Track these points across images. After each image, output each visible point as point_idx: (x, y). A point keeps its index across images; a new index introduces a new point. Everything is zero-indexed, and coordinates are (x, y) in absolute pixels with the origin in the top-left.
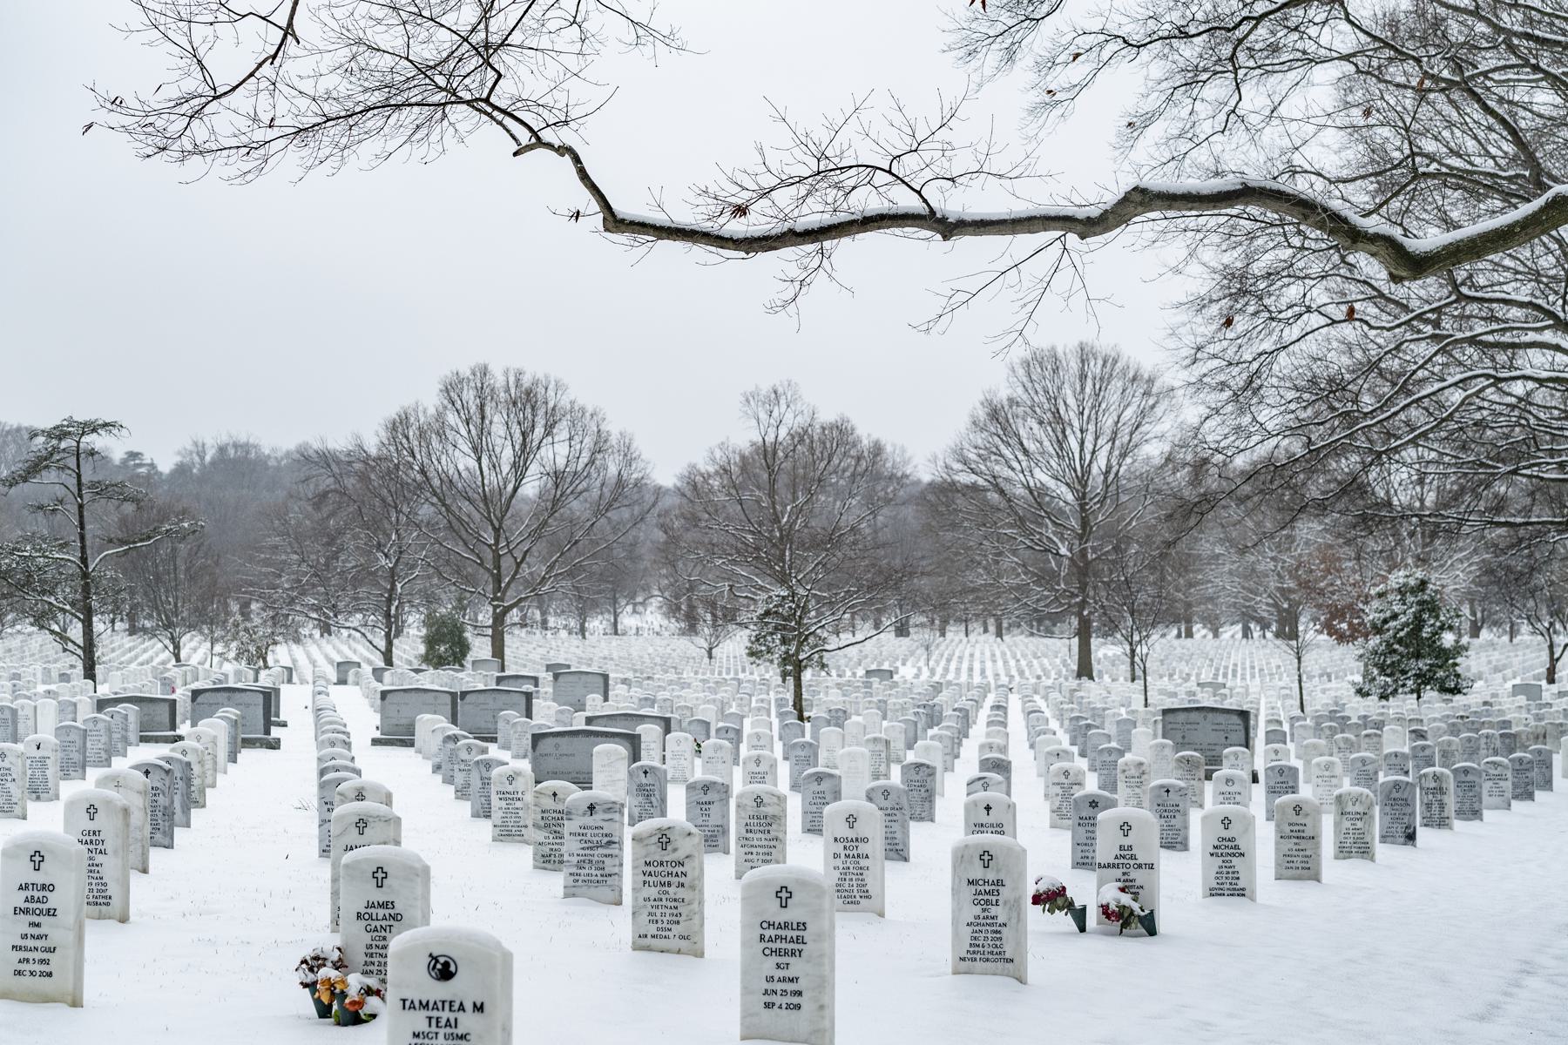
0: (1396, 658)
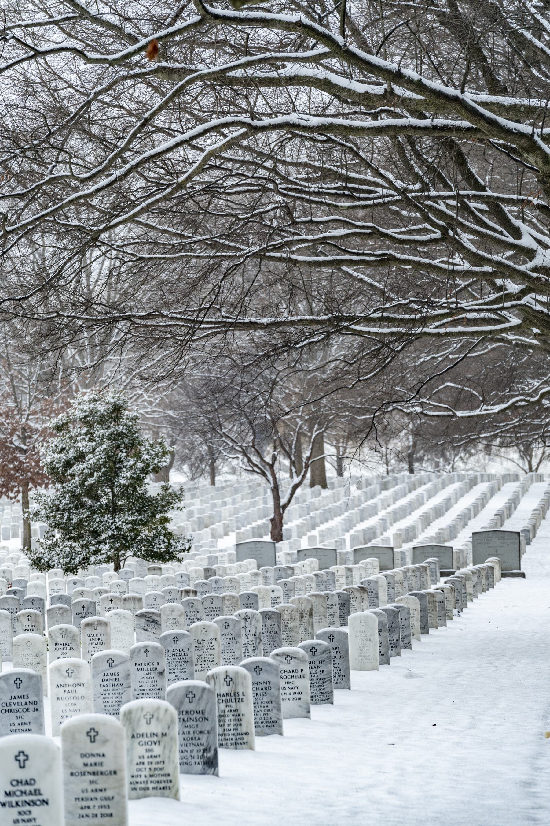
0: (84, 514)
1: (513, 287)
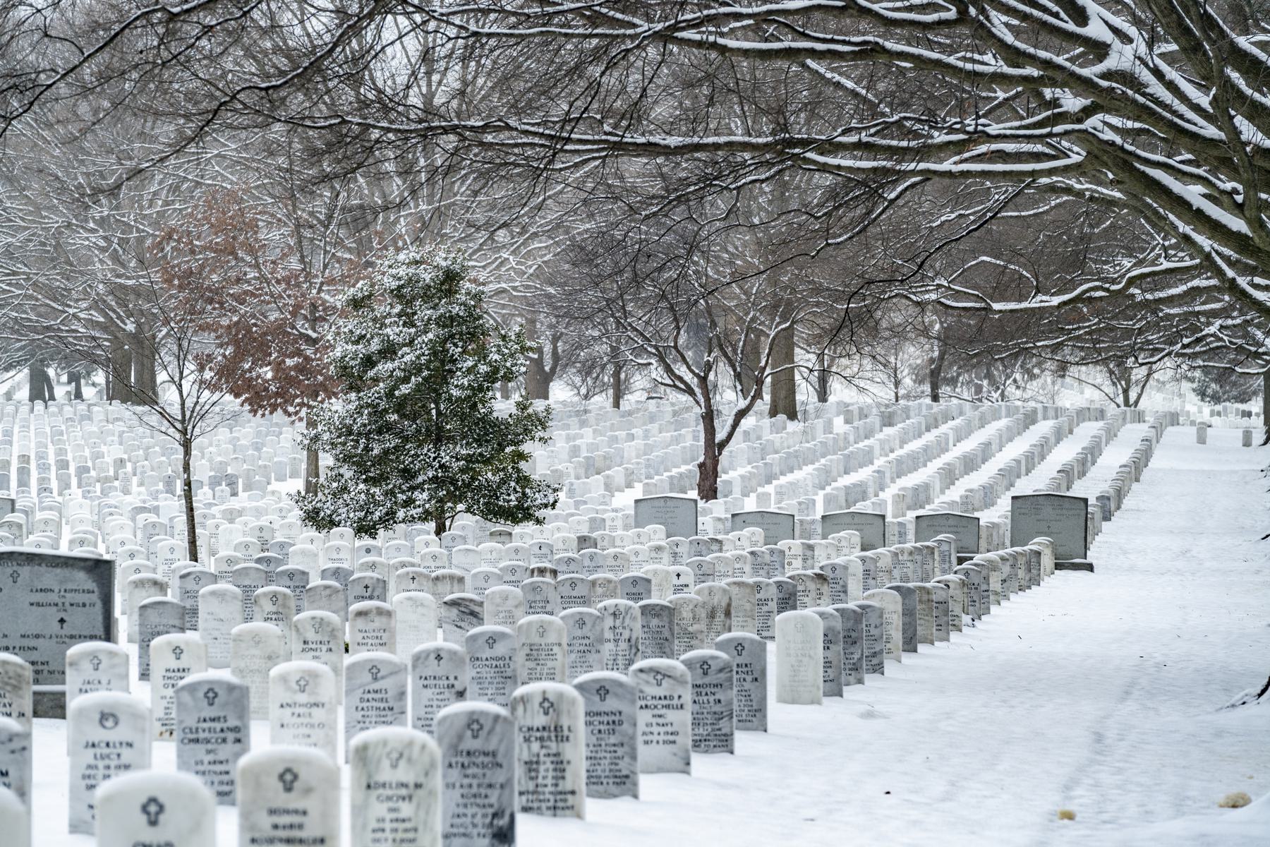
1: (1072, 102)
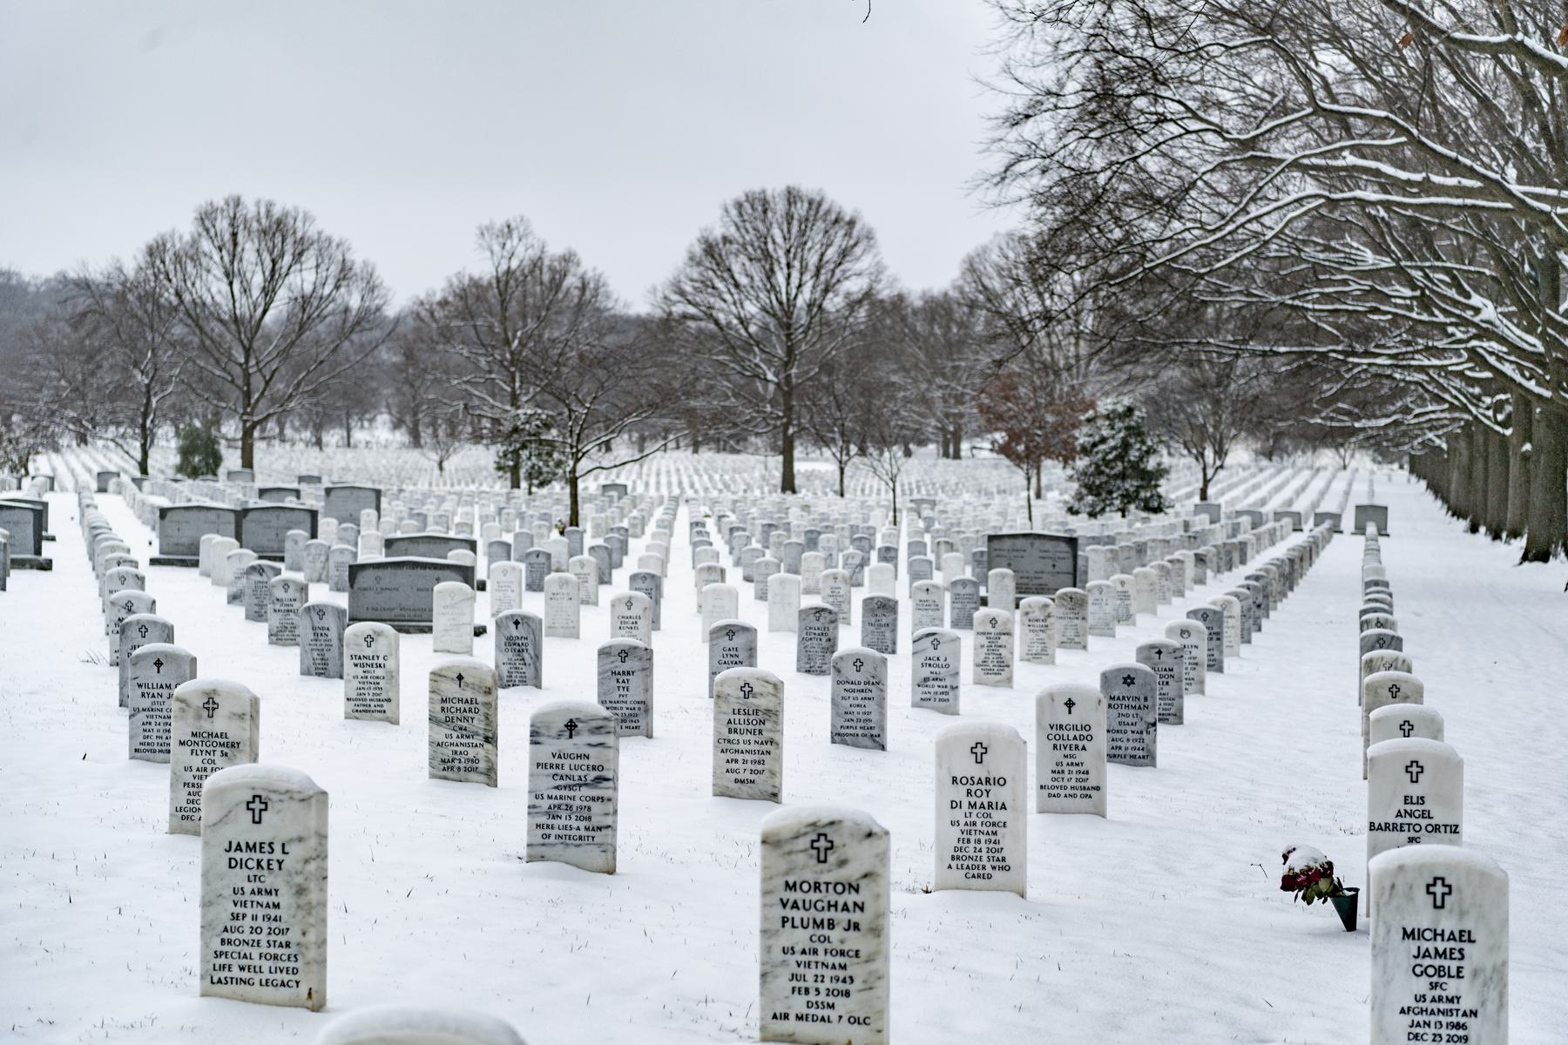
0: (1104, 479)
